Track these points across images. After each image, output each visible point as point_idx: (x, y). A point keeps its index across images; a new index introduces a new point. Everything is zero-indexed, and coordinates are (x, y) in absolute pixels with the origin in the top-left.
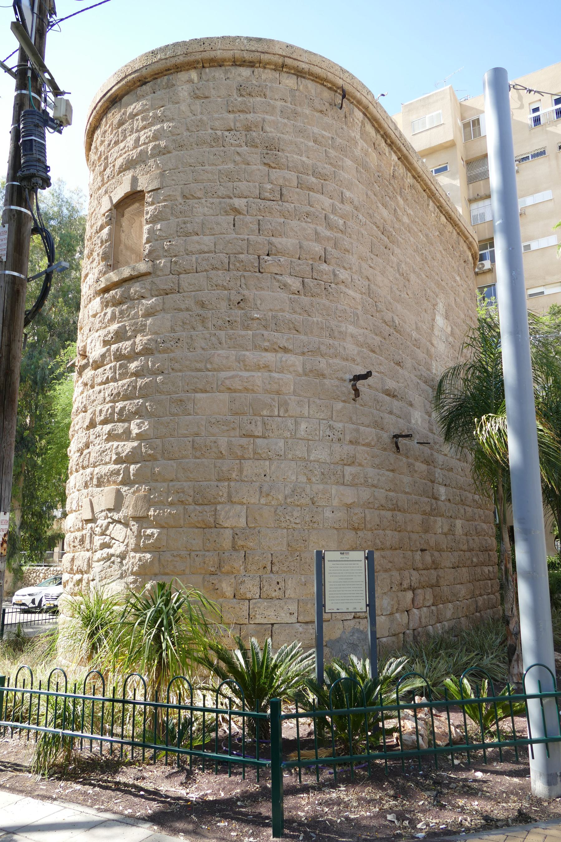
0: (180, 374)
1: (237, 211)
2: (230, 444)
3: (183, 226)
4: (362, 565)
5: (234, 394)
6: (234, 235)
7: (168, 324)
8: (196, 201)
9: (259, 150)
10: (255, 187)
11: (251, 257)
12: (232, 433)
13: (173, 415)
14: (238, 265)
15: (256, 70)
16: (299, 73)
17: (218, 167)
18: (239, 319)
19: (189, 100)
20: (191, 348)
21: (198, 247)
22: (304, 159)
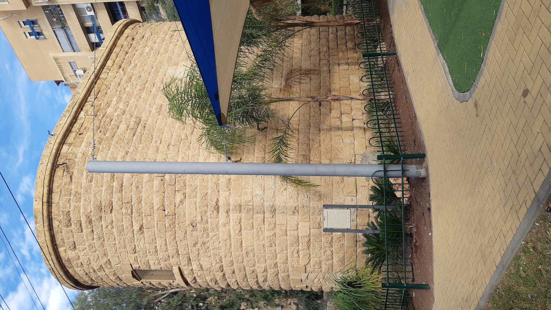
0: (233, 254)
1: (141, 228)
2: (268, 230)
3: (151, 253)
4: (330, 210)
5: (243, 228)
6: (155, 228)
7: (207, 259)
8: (137, 247)
9: (103, 215)
10: (126, 218)
11: (167, 220)
12: (263, 229)
13: (254, 256)
14: (172, 227)
15: (53, 217)
16: (50, 192)
17: (116, 237)
18: (203, 226)
19: (77, 251)
20: (219, 248)
21: (163, 246)
22: (104, 189)
